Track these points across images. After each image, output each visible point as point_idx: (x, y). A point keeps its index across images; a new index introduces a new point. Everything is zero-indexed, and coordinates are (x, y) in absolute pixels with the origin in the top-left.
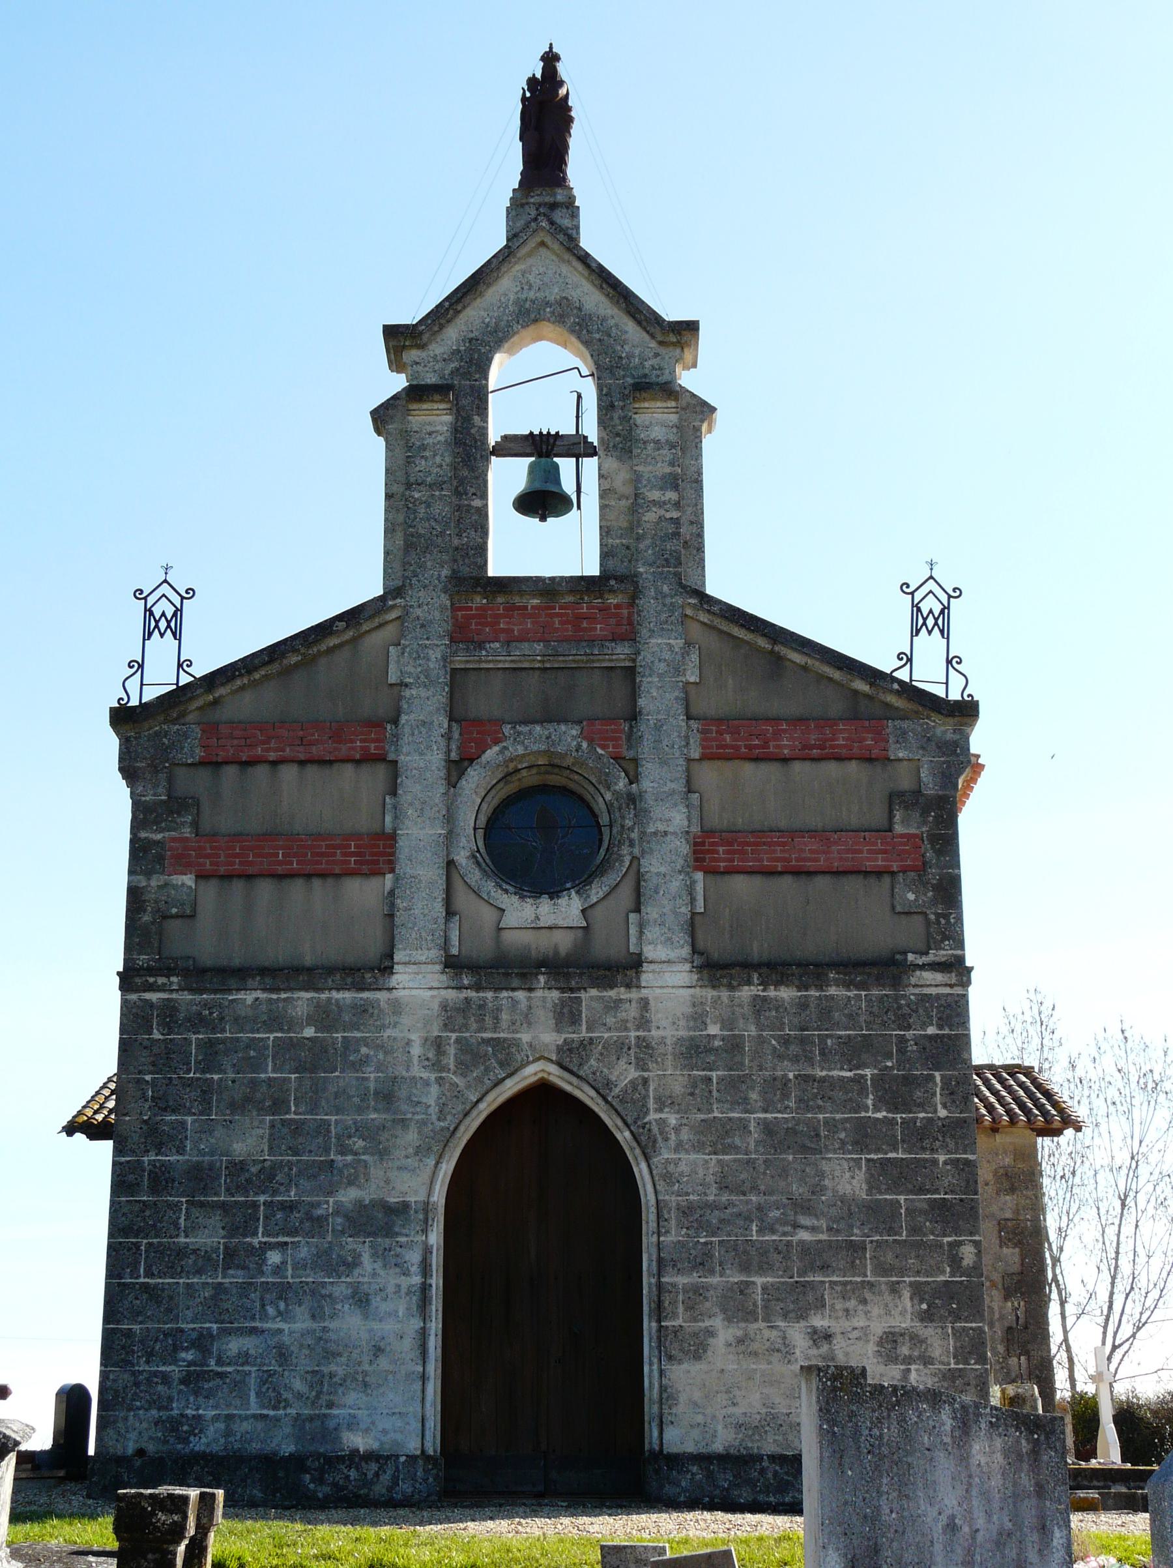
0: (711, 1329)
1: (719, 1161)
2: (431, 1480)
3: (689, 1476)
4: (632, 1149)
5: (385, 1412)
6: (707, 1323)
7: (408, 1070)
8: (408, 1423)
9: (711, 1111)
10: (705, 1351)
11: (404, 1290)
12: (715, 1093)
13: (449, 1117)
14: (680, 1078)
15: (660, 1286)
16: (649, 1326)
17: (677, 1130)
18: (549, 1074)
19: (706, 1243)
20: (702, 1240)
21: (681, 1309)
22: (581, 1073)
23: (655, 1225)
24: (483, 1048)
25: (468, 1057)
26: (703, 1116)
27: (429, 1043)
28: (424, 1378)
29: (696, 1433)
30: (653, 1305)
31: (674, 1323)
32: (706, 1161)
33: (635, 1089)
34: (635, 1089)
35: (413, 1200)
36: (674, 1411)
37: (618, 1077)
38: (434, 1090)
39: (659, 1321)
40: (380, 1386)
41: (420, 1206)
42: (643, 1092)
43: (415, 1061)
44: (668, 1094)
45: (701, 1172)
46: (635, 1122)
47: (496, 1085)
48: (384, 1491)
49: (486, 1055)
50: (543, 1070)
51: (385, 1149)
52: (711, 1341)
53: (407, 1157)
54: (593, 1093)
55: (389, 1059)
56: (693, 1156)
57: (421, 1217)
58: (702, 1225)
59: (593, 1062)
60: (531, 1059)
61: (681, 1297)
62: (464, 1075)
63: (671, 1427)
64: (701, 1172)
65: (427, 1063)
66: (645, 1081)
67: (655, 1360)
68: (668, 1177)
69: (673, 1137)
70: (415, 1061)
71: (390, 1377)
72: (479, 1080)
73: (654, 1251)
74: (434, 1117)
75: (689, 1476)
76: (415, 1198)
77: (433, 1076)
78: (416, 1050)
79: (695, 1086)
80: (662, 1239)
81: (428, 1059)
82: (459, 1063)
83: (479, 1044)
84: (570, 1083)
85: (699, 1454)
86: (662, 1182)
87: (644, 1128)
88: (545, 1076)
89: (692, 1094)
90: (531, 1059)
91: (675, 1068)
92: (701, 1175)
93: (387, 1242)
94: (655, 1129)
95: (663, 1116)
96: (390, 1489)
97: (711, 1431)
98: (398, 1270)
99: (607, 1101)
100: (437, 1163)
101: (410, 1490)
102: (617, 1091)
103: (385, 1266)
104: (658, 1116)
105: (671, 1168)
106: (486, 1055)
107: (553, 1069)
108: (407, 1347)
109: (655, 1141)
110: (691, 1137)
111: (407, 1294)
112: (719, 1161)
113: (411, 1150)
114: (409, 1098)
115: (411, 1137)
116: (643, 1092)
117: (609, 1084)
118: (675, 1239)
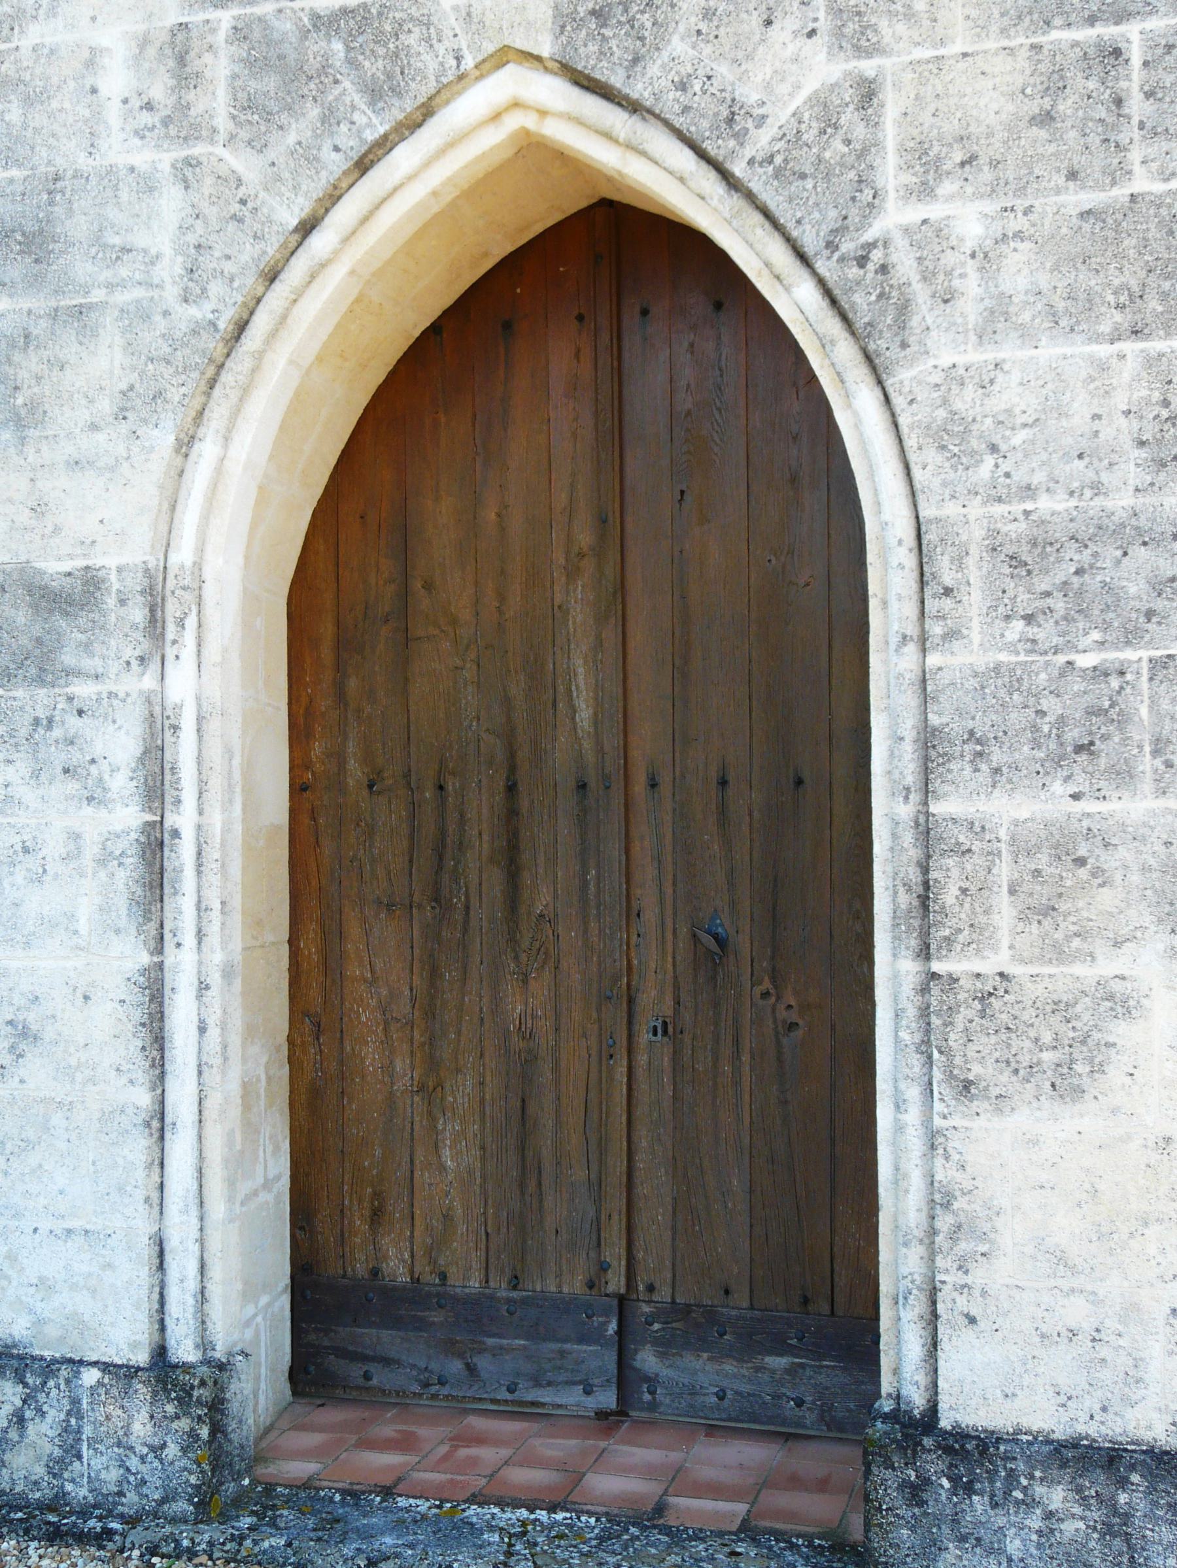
0: (1117, 986)
1: (1151, 362)
2: (172, 1450)
3: (1035, 1521)
4: (824, 344)
5: (45, 1225)
6: (1107, 966)
7: (92, 149)
8: (109, 1266)
9: (1118, 174)
10: (1097, 1069)
11: (91, 850)
12: (1137, 106)
13: (216, 288)
14: (1000, 64)
15: (926, 831)
16: (893, 970)
17: (984, 257)
18: (543, 113)
19: (1100, 673)
20: (1086, 661)
21: (1004, 913)
22: (638, 90)
23: (910, 609)
24: (316, 46)
25: (270, 83)
26: (1080, 199)
27: (151, 51)
28: (159, 1123)
29: (1062, 1365)
30: (904, 899)
31: (978, 966)
32: (1103, 367)
33: (830, 125)
34: (830, 125)
35: (111, 562)
36: (978, 1276)
37: (768, 86)
38: (171, 203)
39: (925, 953)
40: (27, 1145)
41: (135, 582)
42: (860, 132)
43: (113, 114)
44: (951, 127)
45: (1080, 409)
46: (831, 246)
47: (363, 166)
48: (40, 1471)
49: (324, 69)
50: (516, 105)
51: (33, 406)
52: (1120, 1031)
53: (94, 427)
54: (685, 160)
55: (38, 119)
56: (1050, 351)
57: (138, 614)
58: (1082, 603)
59: (678, 46)
60: (469, 62)
61: (1004, 871)
62: (258, 145)
63: (968, 1334)
64: (1080, 409)
65: (146, 118)
66: (867, 93)
67: (913, 1093)
68: (953, 436)
69: (971, 285)
70: (113, 114)
71: (57, 1119)
72: (306, 155)
73: (909, 700)
74: (171, 293)
75: (1035, 1521)
76: (122, 555)
77: (166, 159)
78: (116, 81)
79: (1056, 85)
80: (933, 660)
81: (149, 106)
82: (247, 106)
83: (305, 34)
84: (608, 136)
85: (1074, 1444)
86: (932, 456)
87: (862, 261)
88: (529, 121)
89: (1046, 118)
90: (469, 62)
91: (981, 28)
92: (1079, 418)
93: (40, 700)
94: (905, 266)
95: (934, 211)
96: (57, 1467)
97: (1123, 1361)
98: (73, 786)
99: (725, 175)
100: (186, 444)
101: (113, 1475)
102: (762, 140)
103: (36, 774)
104: (914, 214)
105: (966, 400)
106: (324, 69)
107: (552, 91)
108: (104, 1028)
109: (904, 309)
110: (1044, 280)
111: (102, 862)
112: (1151, 362)
113: (106, 406)
114: (97, 240)
115: (103, 363)
116: (860, 132)
117: (733, 118)
118: (981, 660)
